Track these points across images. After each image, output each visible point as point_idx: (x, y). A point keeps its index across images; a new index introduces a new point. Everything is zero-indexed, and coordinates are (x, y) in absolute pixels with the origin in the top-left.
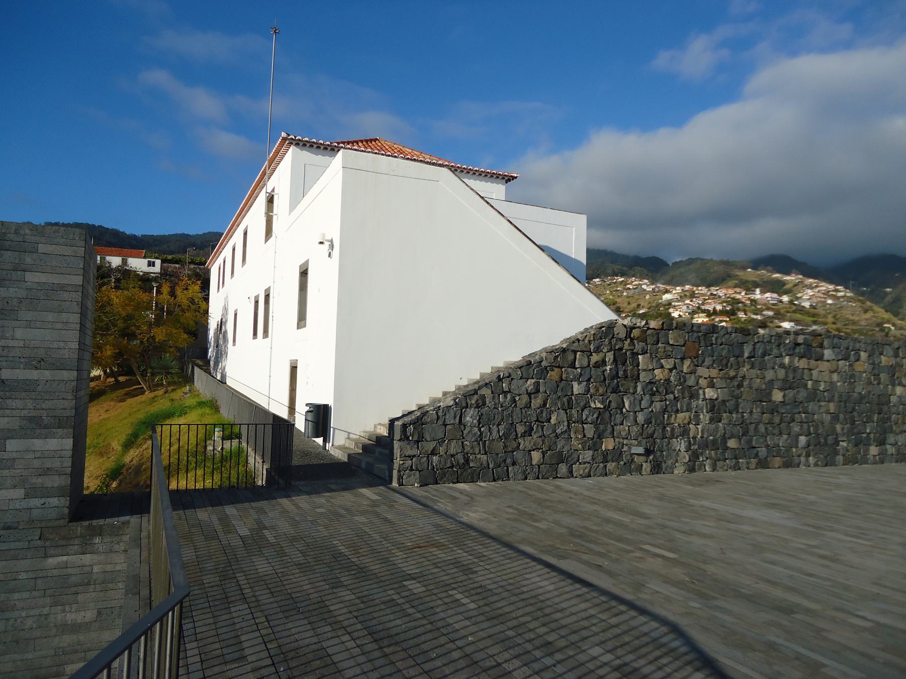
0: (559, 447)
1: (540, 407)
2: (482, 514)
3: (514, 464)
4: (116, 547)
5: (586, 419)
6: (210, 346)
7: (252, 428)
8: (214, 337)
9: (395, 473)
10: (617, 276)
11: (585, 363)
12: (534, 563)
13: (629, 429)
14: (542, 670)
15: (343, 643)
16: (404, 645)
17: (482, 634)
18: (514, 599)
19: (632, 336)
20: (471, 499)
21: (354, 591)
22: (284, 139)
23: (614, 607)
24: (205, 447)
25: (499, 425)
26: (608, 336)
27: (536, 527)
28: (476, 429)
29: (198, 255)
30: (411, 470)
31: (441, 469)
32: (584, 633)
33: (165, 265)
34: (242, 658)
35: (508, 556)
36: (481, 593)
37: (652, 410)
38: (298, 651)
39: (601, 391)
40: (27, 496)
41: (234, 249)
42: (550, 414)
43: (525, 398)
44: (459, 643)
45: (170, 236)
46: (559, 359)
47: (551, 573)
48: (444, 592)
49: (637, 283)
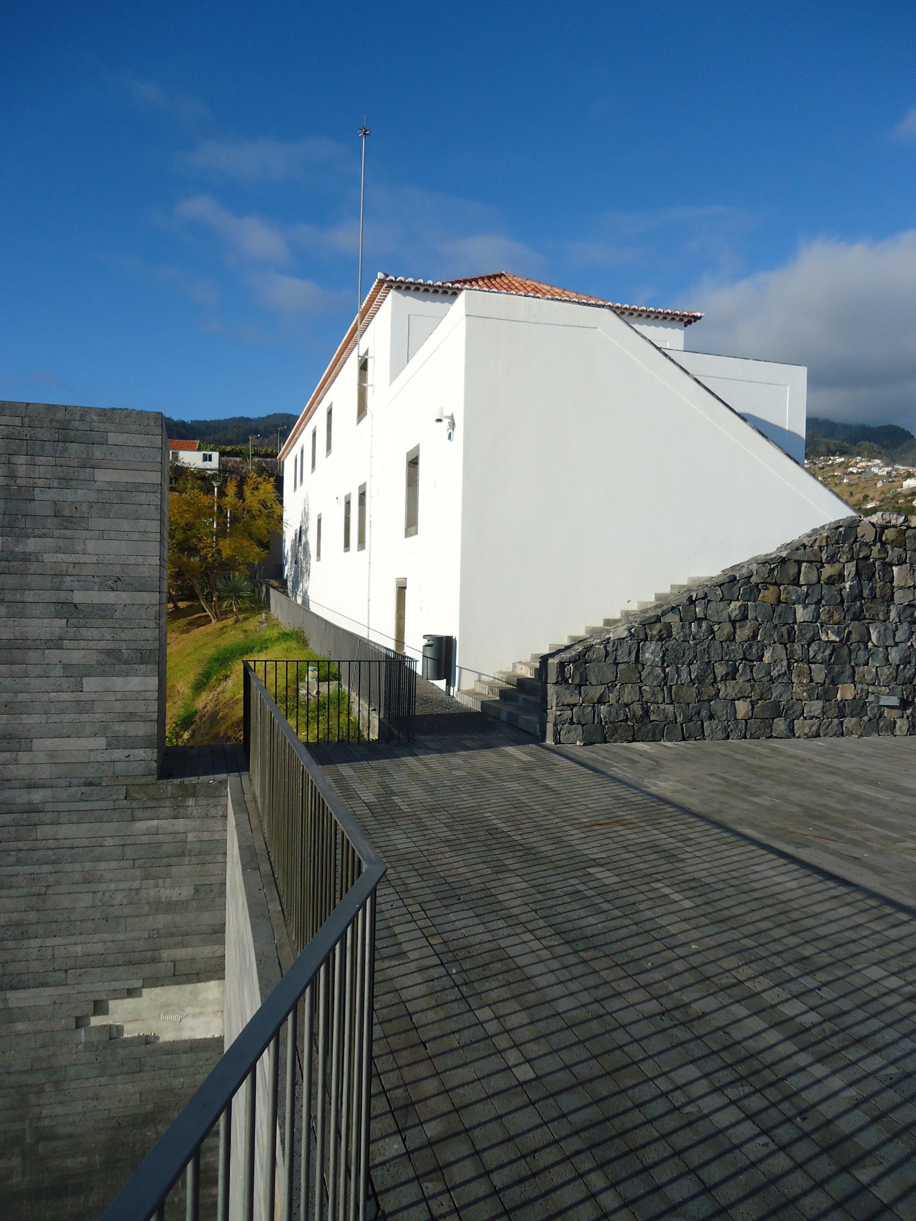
0: (774, 695)
1: (749, 640)
2: (676, 784)
3: (711, 717)
4: (213, 812)
5: (814, 656)
6: (287, 561)
7: (354, 665)
8: (292, 551)
9: (550, 728)
10: (834, 455)
11: (814, 579)
12: (762, 852)
13: (877, 671)
14: (803, 994)
15: (525, 942)
16: (607, 950)
17: (711, 942)
18: (744, 897)
19: (884, 539)
20: (657, 765)
21: (526, 878)
22: (382, 282)
23: (889, 915)
24: (297, 690)
25: (689, 664)
26: (849, 539)
27: (755, 804)
28: (659, 670)
29: (261, 445)
30: (572, 723)
31: (611, 723)
32: (854, 948)
33: (223, 458)
34: (401, 954)
35: (723, 841)
36: (696, 887)
37: (912, 645)
38: (470, 949)
39: (836, 617)
40: (109, 746)
41: (314, 435)
42: (763, 650)
43: (727, 628)
44: (681, 952)
45: (226, 421)
46: (775, 573)
47: (789, 866)
48: (645, 884)
49: (863, 464)
